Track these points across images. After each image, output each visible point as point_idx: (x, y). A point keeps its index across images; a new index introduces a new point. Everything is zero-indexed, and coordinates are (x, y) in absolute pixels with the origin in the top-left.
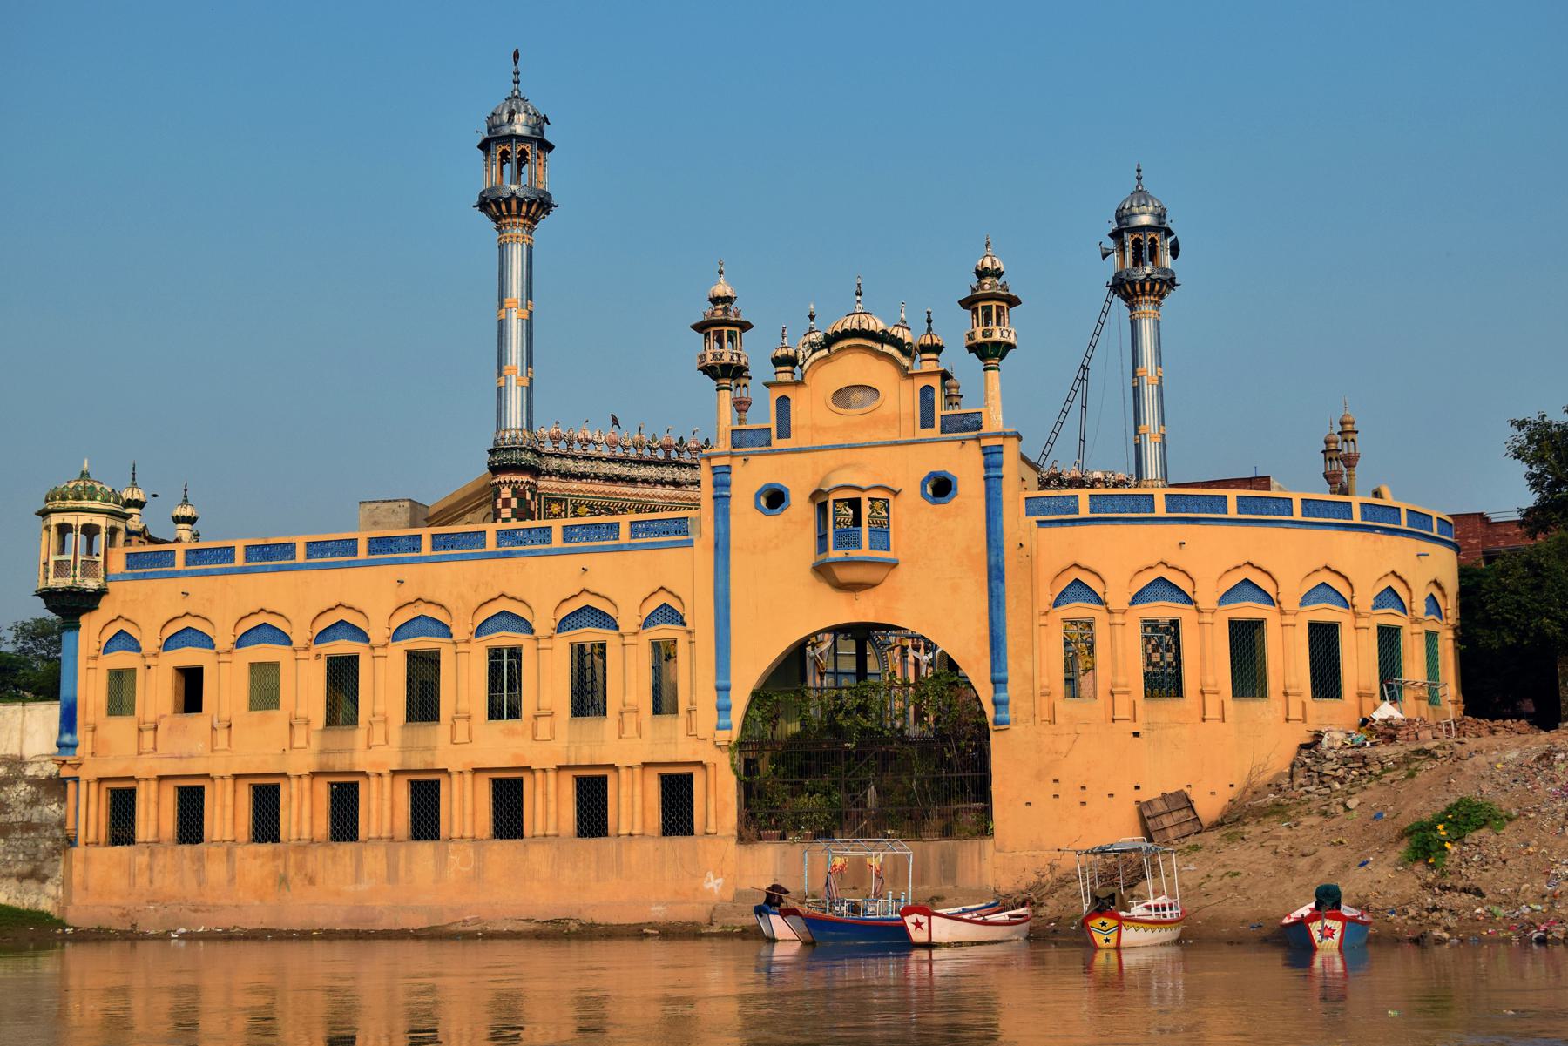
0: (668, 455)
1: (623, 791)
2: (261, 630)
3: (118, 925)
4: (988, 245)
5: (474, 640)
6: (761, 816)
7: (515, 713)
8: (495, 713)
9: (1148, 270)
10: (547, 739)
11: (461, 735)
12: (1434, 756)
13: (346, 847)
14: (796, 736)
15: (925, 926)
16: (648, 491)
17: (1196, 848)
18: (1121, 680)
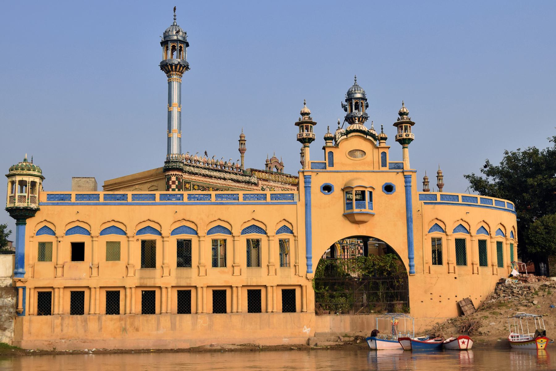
2: (111, 228)
4: (403, 104)
5: (207, 236)
6: (323, 305)
11: (202, 272)
13: (150, 317)
15: (466, 343)
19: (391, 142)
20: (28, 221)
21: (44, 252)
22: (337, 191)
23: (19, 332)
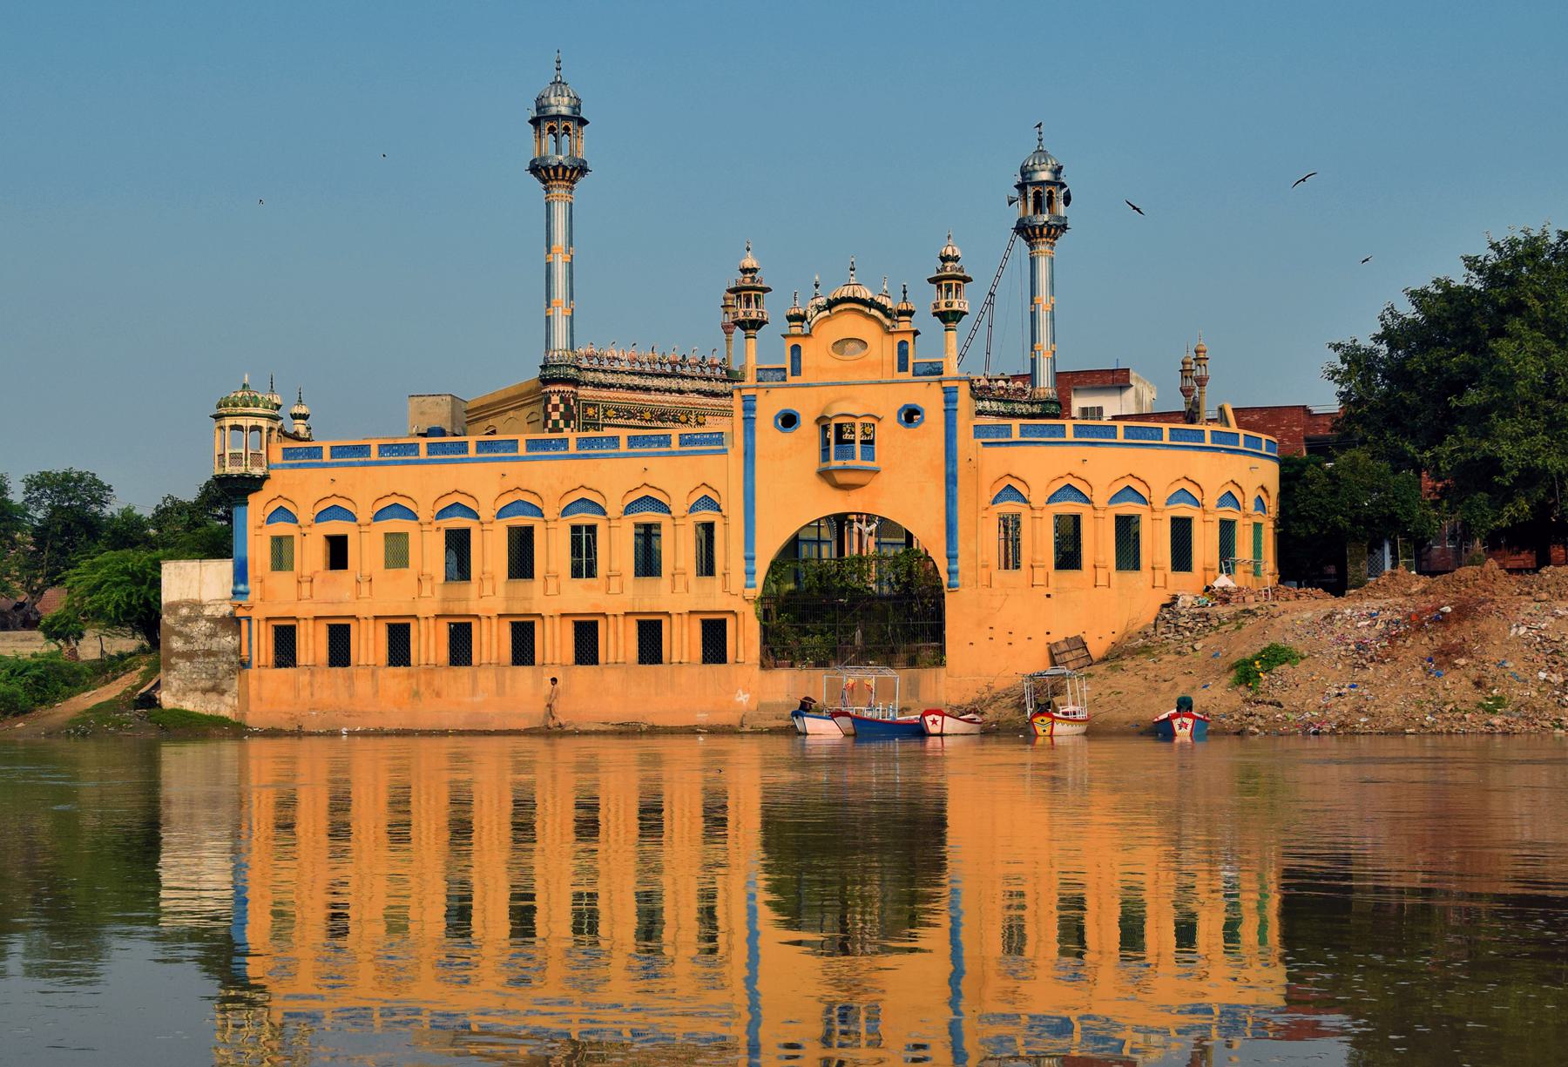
0: (674, 369)
1: (675, 631)
3: (287, 728)
6: (775, 651)
7: (591, 573)
8: (576, 573)
9: (1046, 217)
10: (616, 593)
11: (552, 589)
12: (1255, 614)
14: (791, 593)
16: (659, 397)
17: (1090, 675)
18: (1039, 557)
19: (925, 320)
20: (251, 498)
21: (281, 553)
22: (807, 425)
23: (243, 696)
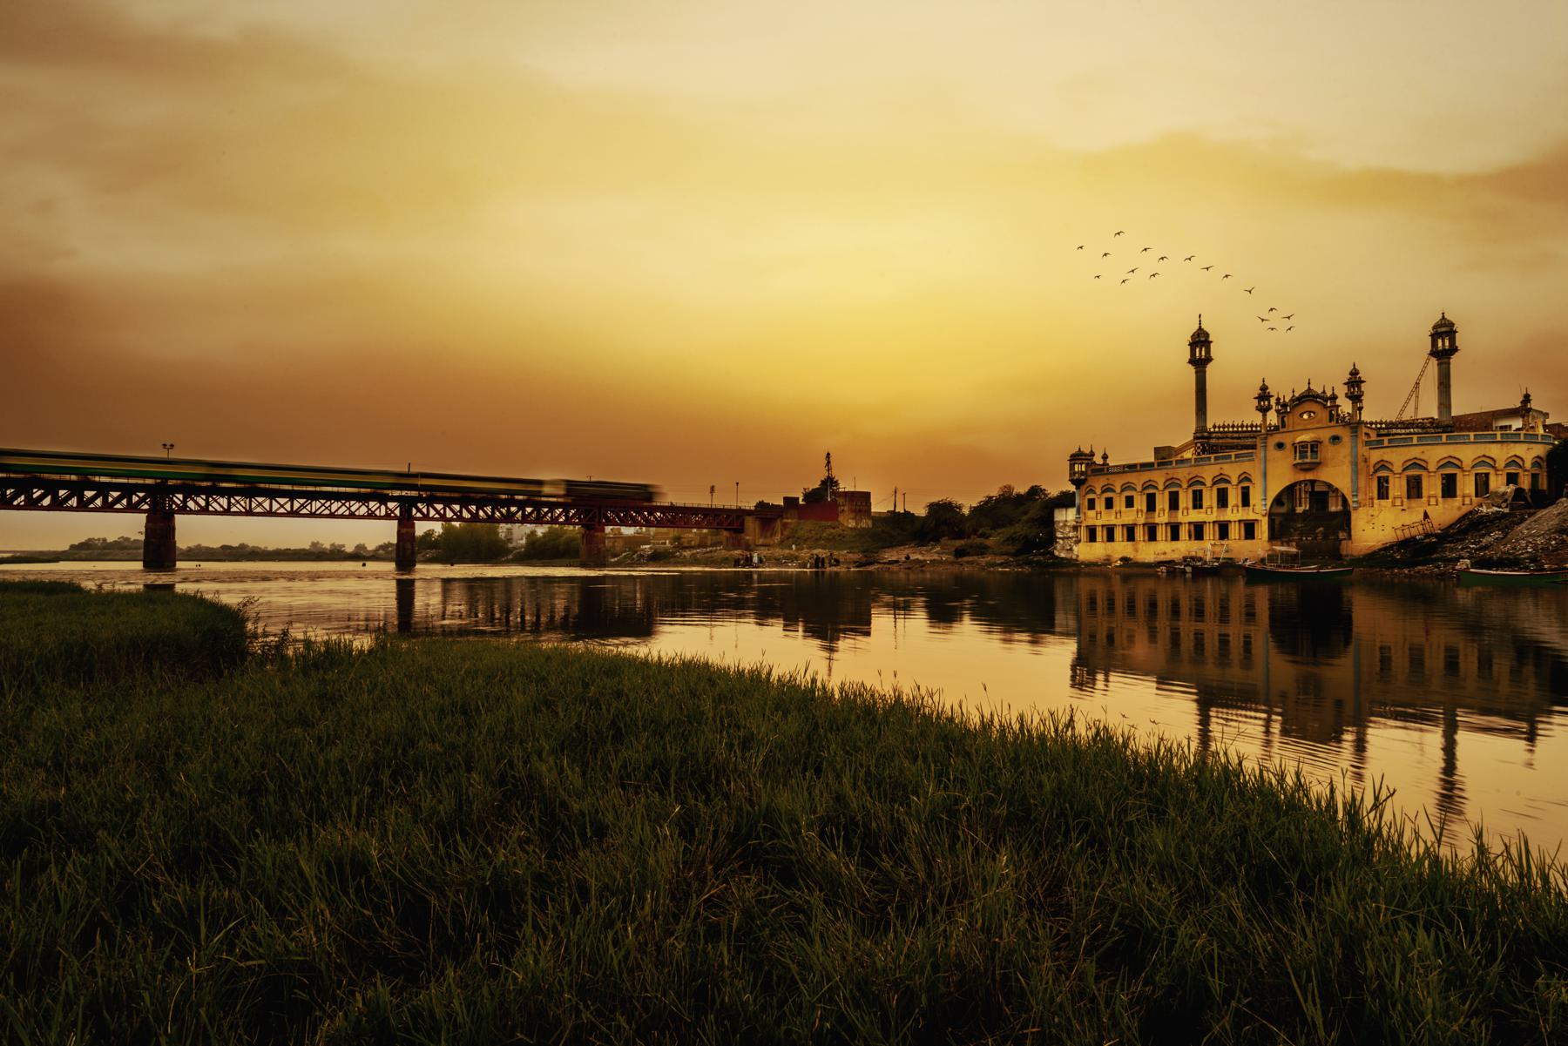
8: (1195, 507)
